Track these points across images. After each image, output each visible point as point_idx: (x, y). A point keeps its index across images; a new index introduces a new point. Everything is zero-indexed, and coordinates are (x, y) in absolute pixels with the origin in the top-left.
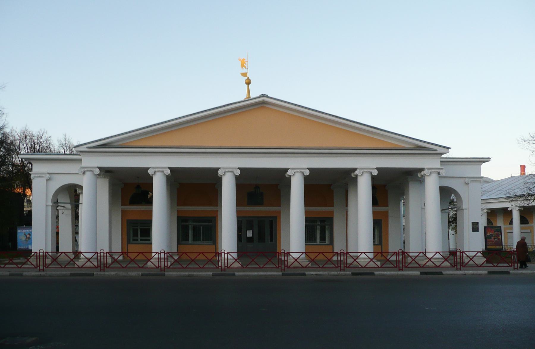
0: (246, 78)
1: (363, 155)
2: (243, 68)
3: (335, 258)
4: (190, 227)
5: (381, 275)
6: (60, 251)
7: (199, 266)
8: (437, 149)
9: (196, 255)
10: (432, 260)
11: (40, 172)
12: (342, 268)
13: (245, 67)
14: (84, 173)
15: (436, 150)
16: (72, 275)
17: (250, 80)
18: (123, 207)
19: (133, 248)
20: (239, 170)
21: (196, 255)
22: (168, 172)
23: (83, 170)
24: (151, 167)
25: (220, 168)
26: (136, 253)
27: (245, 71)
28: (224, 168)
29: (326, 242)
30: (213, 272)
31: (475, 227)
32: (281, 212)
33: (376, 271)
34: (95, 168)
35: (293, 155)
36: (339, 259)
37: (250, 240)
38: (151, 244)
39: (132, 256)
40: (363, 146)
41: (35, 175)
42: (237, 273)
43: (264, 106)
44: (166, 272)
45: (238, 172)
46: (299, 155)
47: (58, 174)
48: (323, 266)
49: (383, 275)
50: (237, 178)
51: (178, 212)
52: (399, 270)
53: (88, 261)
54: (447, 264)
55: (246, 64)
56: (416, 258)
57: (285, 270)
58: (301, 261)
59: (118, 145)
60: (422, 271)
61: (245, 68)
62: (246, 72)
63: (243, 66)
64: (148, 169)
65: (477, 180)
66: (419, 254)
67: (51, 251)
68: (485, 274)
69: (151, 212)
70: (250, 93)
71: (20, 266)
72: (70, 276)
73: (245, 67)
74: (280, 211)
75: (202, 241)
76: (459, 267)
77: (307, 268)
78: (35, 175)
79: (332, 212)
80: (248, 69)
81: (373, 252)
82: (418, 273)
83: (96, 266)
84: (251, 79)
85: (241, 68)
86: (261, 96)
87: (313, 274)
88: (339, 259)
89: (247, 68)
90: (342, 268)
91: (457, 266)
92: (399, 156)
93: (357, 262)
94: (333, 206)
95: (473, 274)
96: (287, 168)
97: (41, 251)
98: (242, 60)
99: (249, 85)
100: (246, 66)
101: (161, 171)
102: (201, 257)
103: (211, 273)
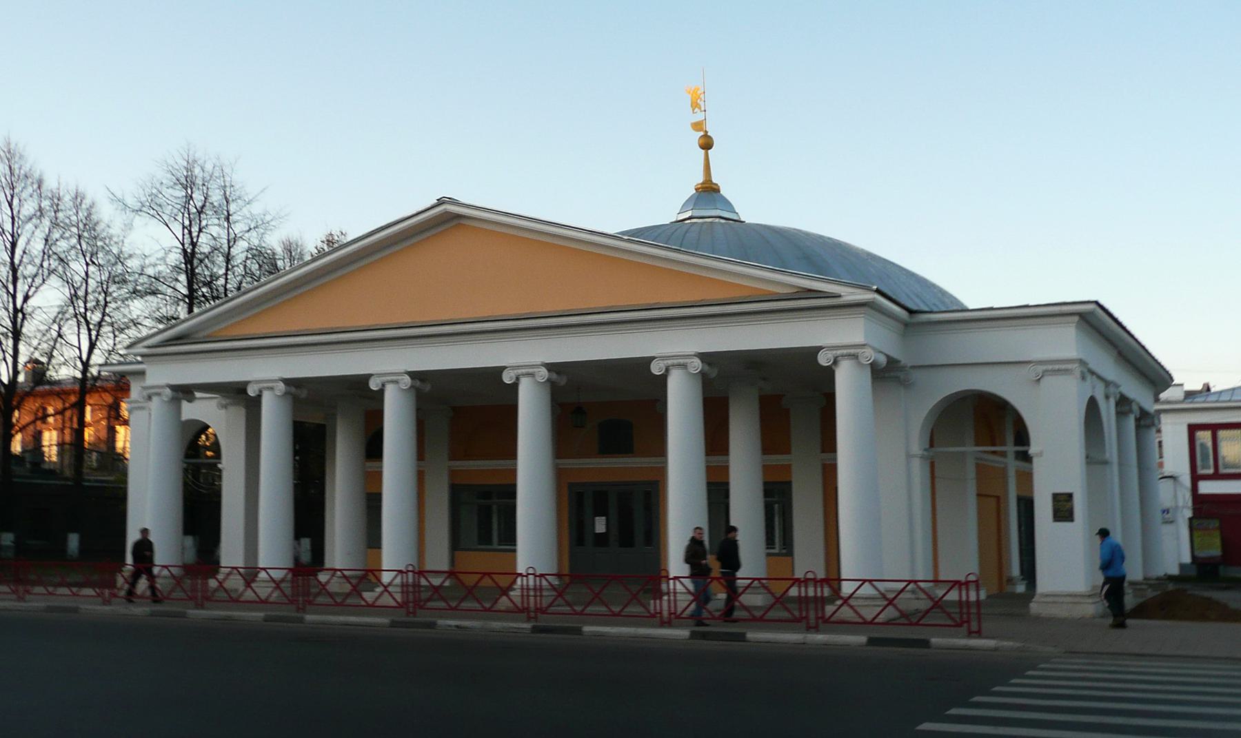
0: (702, 133)
1: (381, 343)
2: (696, 110)
3: (794, 592)
4: (495, 508)
5: (341, 625)
6: (327, 565)
7: (447, 603)
8: (842, 294)
9: (476, 577)
10: (851, 602)
11: (1055, 359)
12: (812, 621)
13: (700, 108)
14: (150, 398)
15: (840, 296)
16: (50, 609)
17: (710, 137)
18: (453, 463)
19: (476, 561)
20: (408, 377)
21: (476, 577)
22: (543, 374)
23: (145, 393)
24: (656, 355)
25: (654, 358)
26: (787, 581)
27: (699, 117)
28: (380, 375)
29: (774, 548)
30: (269, 613)
31: (1063, 508)
32: (793, 467)
33: (441, 617)
34: (162, 387)
35: (784, 315)
36: (964, 598)
37: (601, 539)
38: (515, 551)
39: (470, 580)
40: (281, 330)
41: (1045, 367)
42: (440, 622)
43: (459, 224)
44: (308, 614)
45: (697, 365)
46: (592, 329)
47: (995, 366)
48: (623, 609)
49: (602, 635)
50: (553, 386)
51: (453, 473)
52: (809, 629)
53: (888, 605)
54: (178, 594)
55: (701, 99)
56: (900, 597)
57: (536, 618)
58: (861, 602)
59: (204, 337)
60: (876, 635)
61: (699, 111)
62: (701, 120)
63: (695, 105)
64: (369, 376)
65: (1063, 367)
66: (907, 586)
67: (246, 562)
68: (859, 646)
69: (513, 472)
70: (711, 165)
71: (74, 590)
72: (389, 627)
73: (700, 108)
74: (790, 466)
75: (495, 546)
76: (974, 626)
77: (492, 611)
78: (1045, 367)
79: (788, 468)
80: (705, 111)
81: (554, 572)
82: (684, 633)
83: (517, 607)
84: (713, 138)
85: (691, 109)
86: (441, 202)
87: (450, 626)
88: (964, 598)
89: (703, 109)
90: (812, 621)
91: (968, 622)
92: (361, 345)
93: (852, 607)
94: (788, 451)
95: (826, 644)
96: (817, 347)
97: (810, 577)
98: (694, 91)
99: (709, 151)
100: (702, 103)
101: (849, 355)
102: (487, 582)
103: (262, 614)
